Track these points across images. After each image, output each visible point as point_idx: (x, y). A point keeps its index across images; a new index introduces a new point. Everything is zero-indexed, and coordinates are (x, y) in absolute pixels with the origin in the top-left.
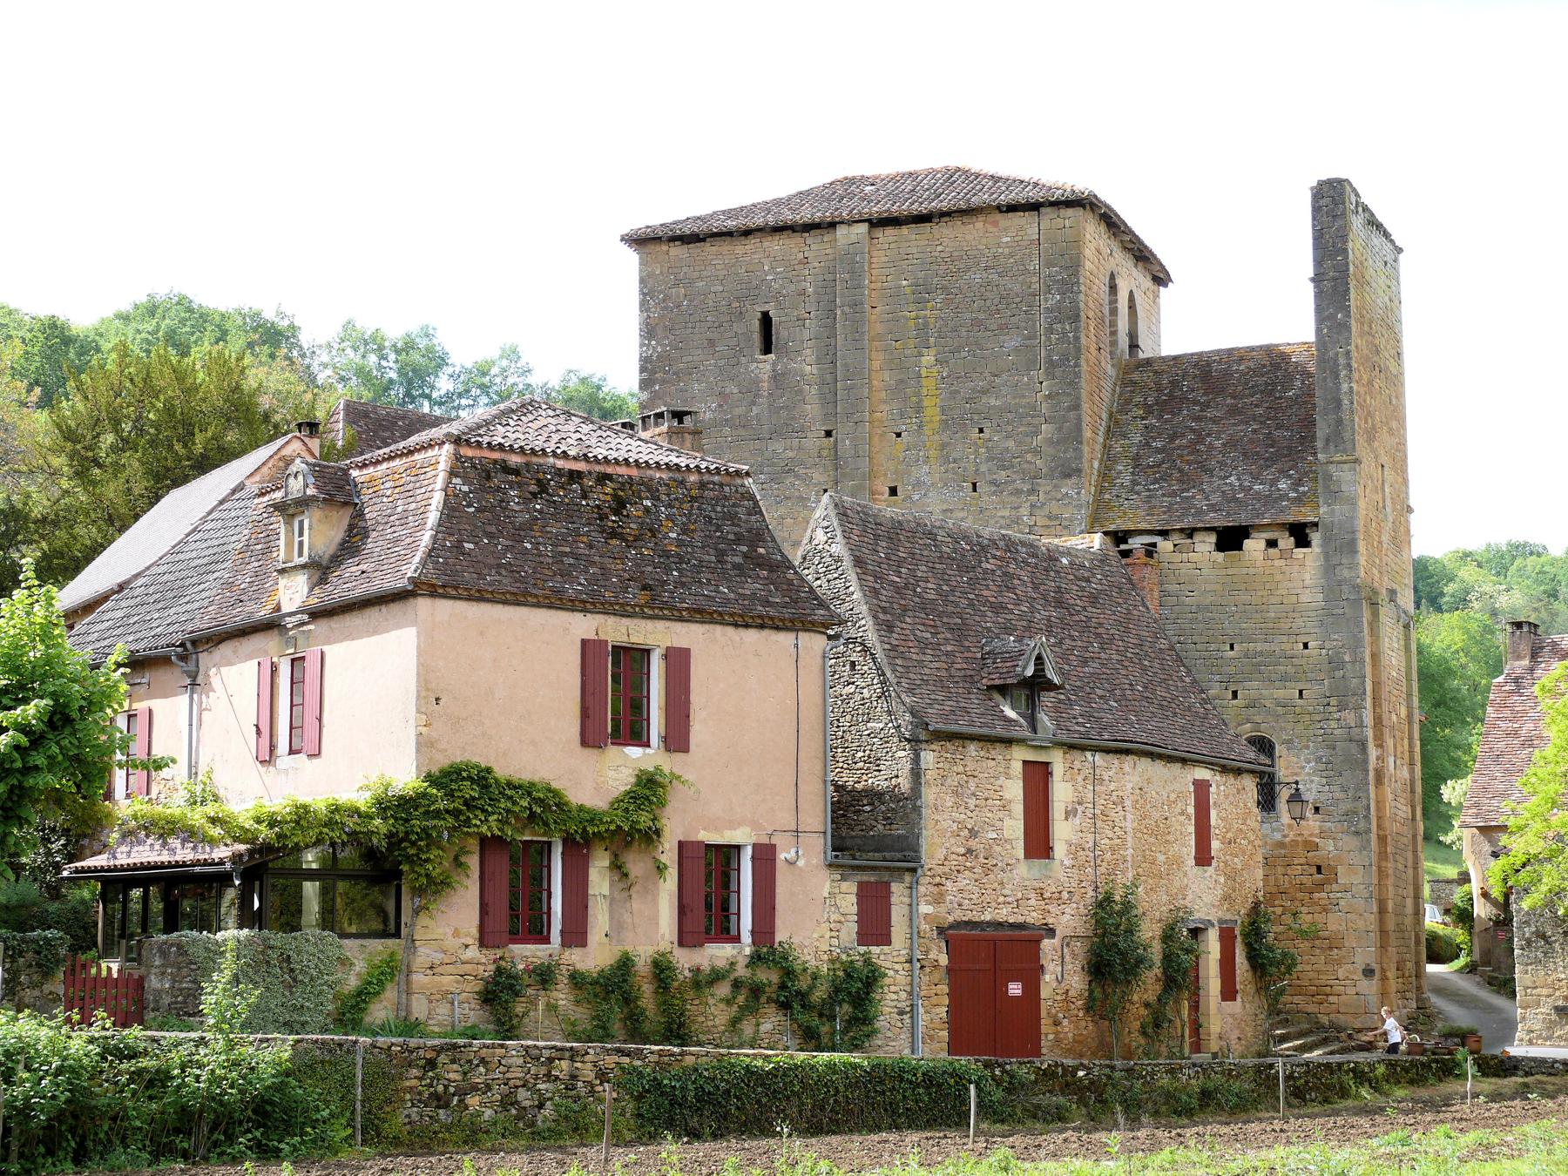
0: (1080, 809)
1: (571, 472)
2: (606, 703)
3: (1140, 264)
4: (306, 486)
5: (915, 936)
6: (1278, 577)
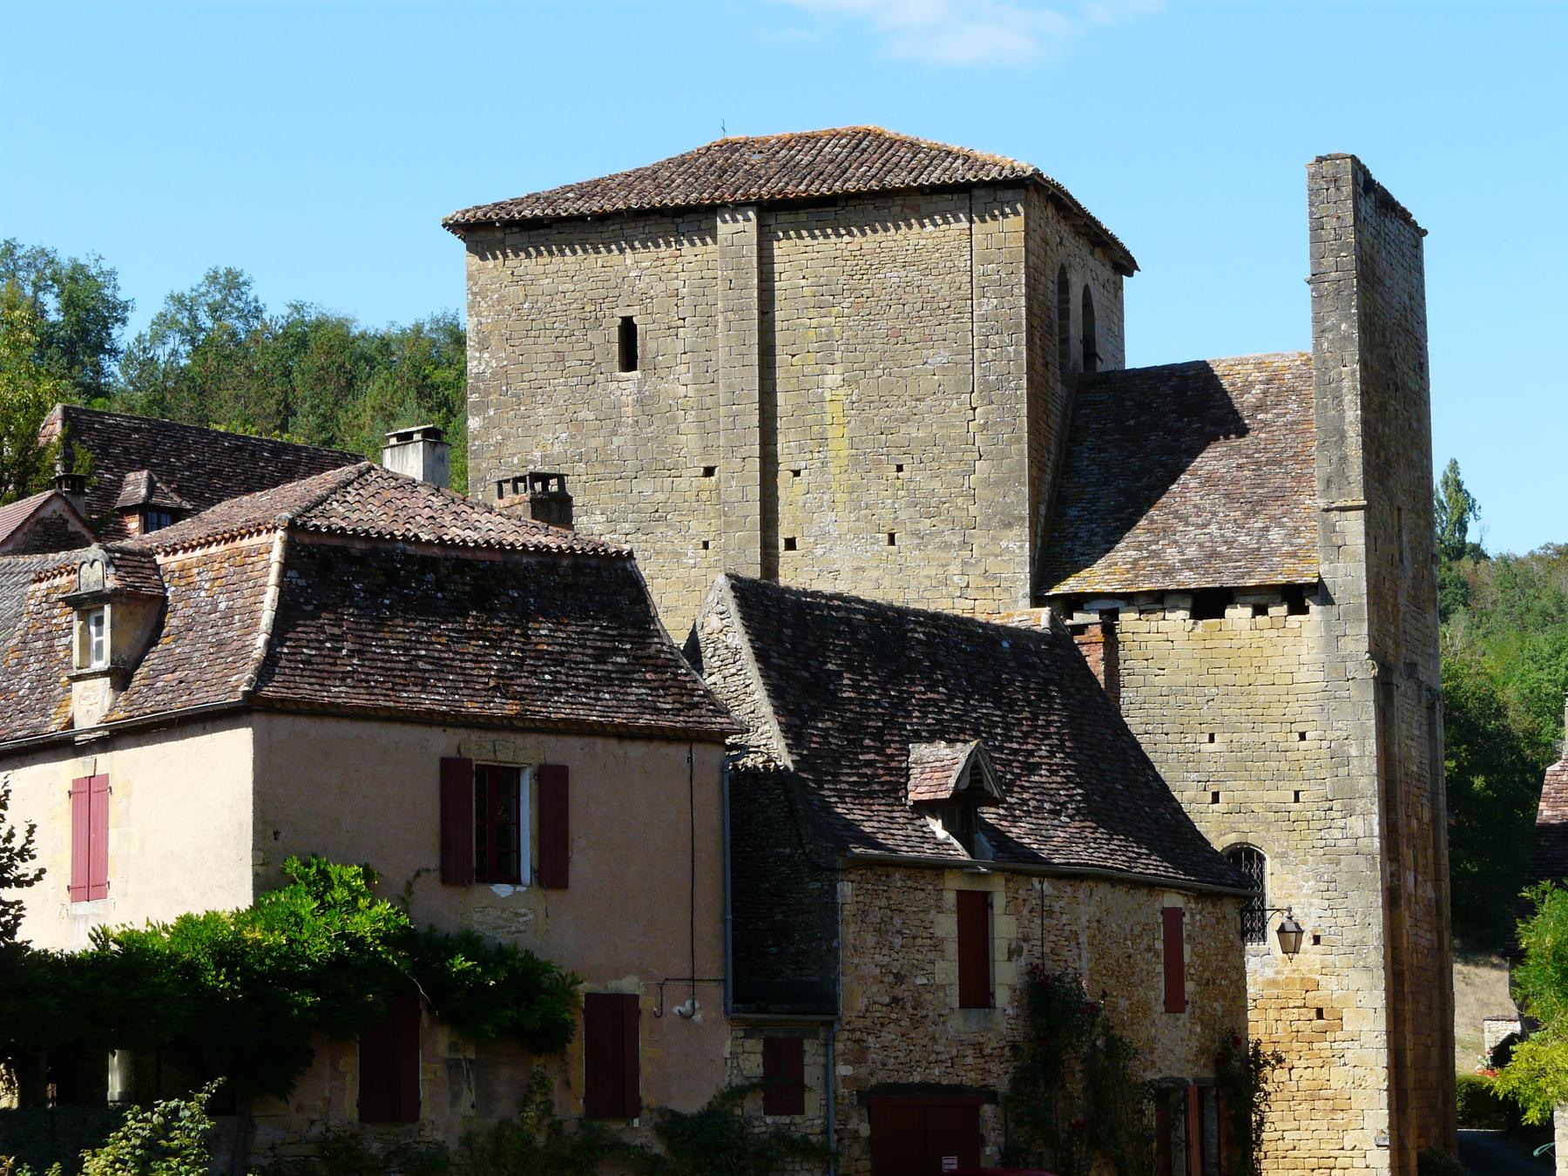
0: (1026, 947)
1: (423, 558)
2: (471, 840)
3: (1098, 251)
4: (105, 577)
5: (832, 1103)
6: (1267, 652)
